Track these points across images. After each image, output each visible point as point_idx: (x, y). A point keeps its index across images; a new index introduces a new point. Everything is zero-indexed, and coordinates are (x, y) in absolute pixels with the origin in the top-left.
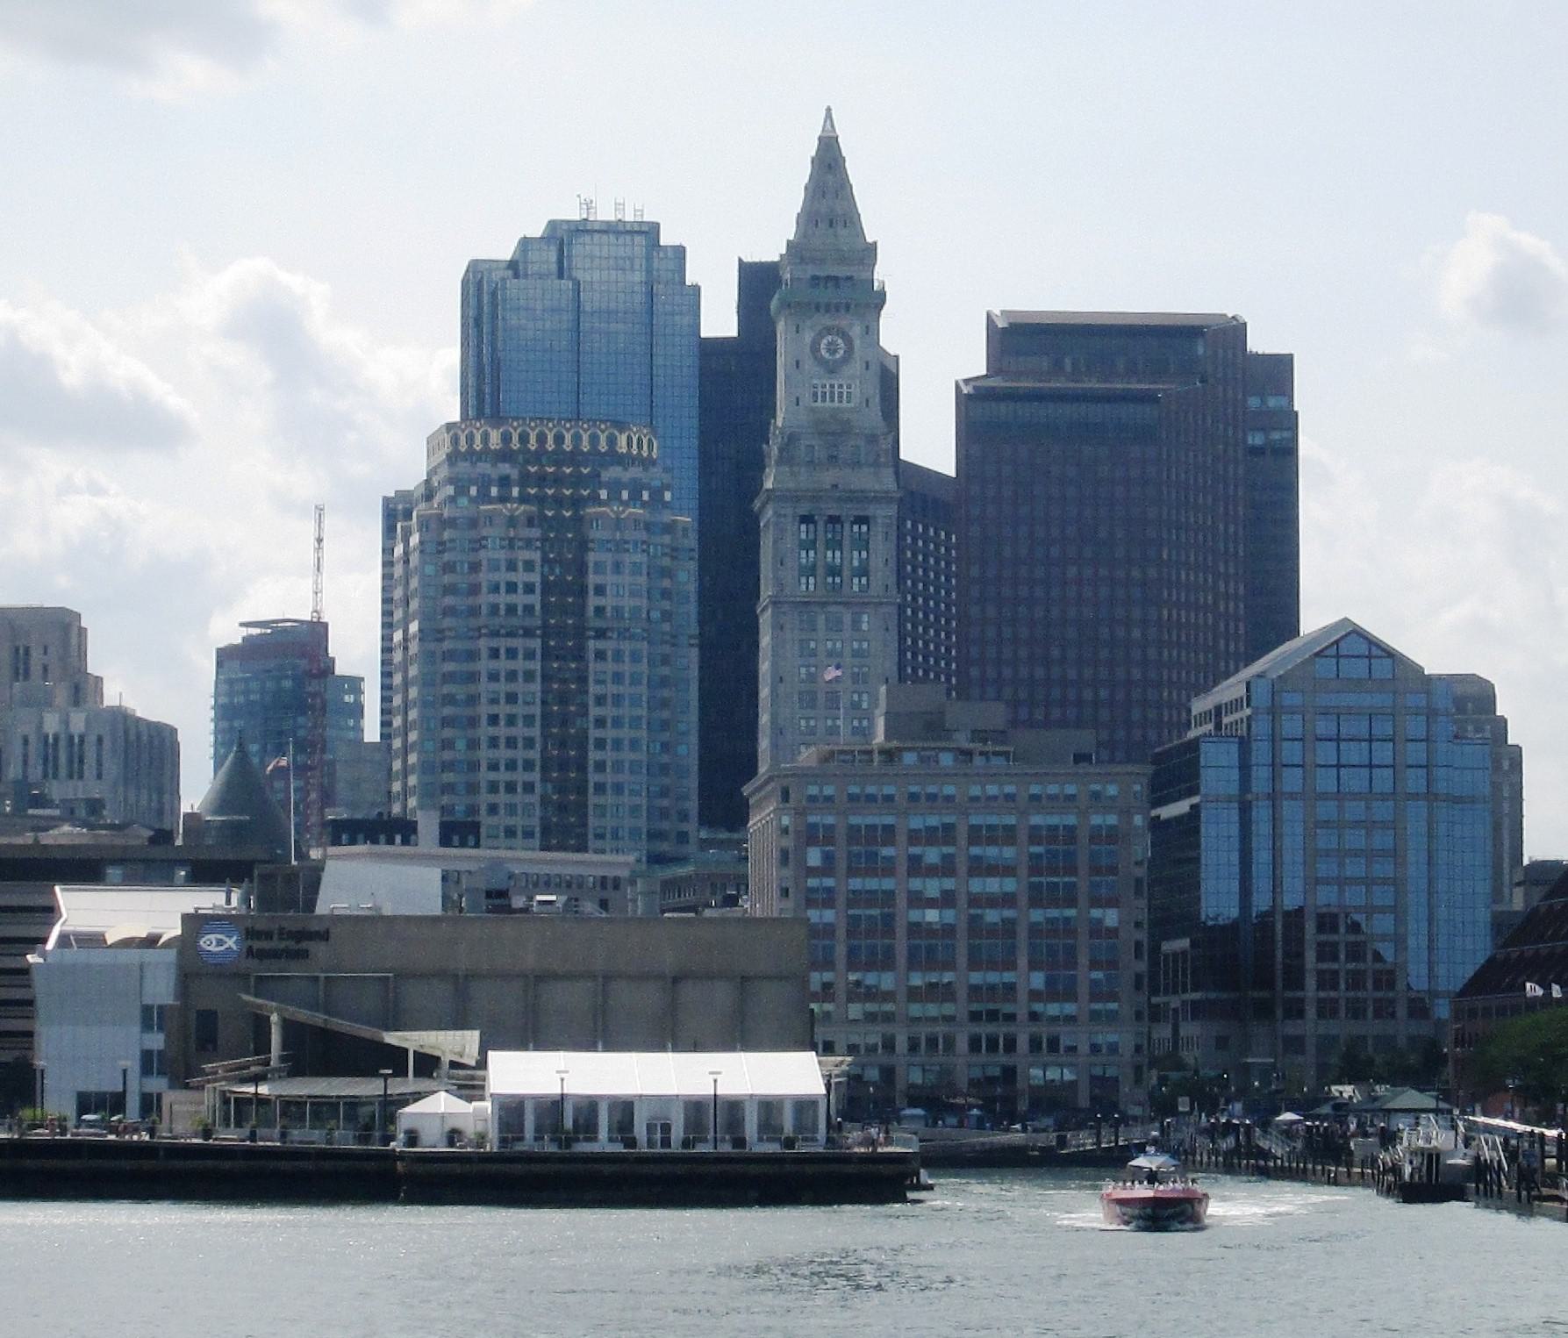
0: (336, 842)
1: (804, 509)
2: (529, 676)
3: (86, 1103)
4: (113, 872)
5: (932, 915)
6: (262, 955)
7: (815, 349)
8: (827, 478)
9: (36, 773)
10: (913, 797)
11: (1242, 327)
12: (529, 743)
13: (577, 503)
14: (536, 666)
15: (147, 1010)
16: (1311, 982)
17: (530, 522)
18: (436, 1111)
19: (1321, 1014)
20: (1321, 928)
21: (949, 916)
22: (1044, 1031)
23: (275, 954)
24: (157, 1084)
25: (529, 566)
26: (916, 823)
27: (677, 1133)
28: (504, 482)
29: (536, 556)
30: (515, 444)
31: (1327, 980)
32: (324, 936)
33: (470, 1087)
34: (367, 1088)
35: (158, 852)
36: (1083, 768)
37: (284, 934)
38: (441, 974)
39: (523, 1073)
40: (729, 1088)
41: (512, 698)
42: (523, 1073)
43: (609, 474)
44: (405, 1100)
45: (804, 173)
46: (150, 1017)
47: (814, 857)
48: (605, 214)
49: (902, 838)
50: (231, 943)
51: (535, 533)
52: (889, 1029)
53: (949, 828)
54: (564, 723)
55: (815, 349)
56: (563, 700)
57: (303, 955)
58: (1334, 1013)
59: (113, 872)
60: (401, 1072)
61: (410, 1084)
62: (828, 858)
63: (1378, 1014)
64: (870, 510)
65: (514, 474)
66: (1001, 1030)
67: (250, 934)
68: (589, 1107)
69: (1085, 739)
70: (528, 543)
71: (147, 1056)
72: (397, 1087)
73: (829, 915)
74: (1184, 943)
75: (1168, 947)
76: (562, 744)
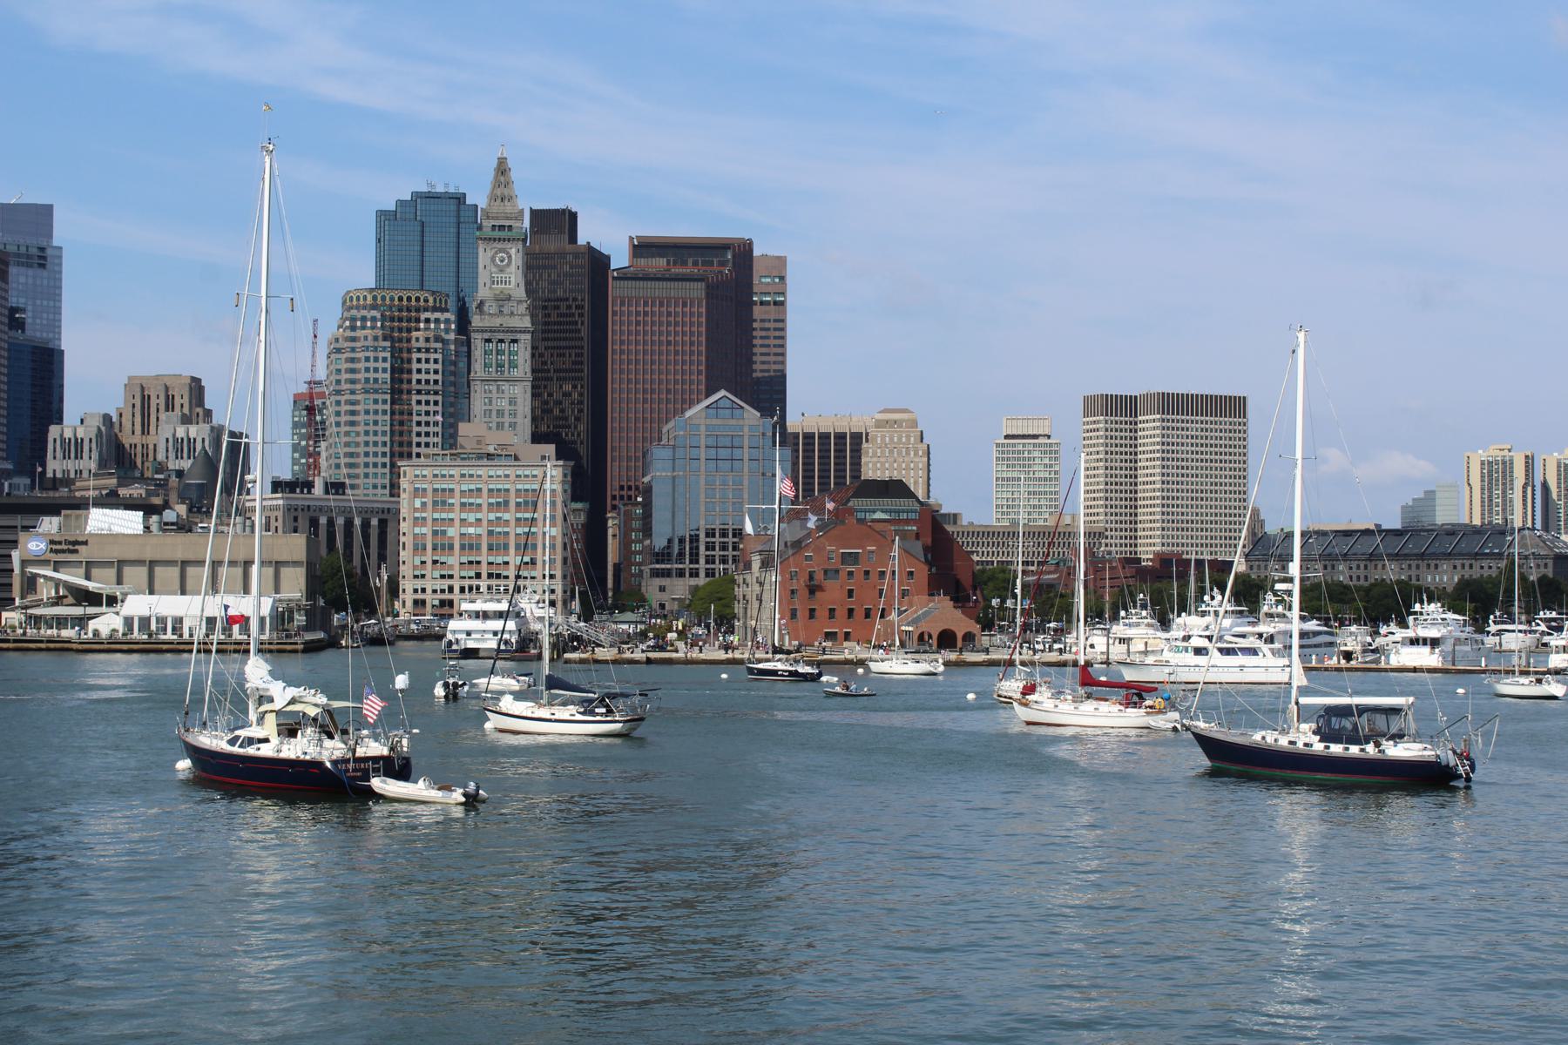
1: (486, 336)
2: (385, 412)
5: (471, 530)
6: (57, 551)
7: (493, 259)
8: (497, 322)
12: (385, 444)
13: (409, 330)
14: (388, 407)
16: (702, 561)
17: (385, 339)
18: (106, 623)
19: (707, 575)
20: (707, 535)
21: (479, 531)
23: (63, 551)
25: (385, 360)
26: (464, 488)
28: (374, 319)
29: (388, 355)
30: (379, 302)
32: (86, 543)
37: (67, 542)
38: (109, 564)
41: (376, 423)
42: (137, 605)
43: (423, 316)
45: (492, 174)
47: (418, 504)
48: (440, 189)
49: (457, 494)
50: (43, 546)
51: (388, 344)
52: (450, 582)
53: (479, 490)
54: (401, 434)
55: (493, 259)
56: (401, 423)
57: (76, 551)
58: (697, 575)
61: (104, 609)
62: (424, 504)
63: (691, 575)
64: (518, 336)
65: (378, 315)
66: (502, 582)
68: (162, 621)
70: (384, 349)
73: (424, 530)
76: (401, 444)
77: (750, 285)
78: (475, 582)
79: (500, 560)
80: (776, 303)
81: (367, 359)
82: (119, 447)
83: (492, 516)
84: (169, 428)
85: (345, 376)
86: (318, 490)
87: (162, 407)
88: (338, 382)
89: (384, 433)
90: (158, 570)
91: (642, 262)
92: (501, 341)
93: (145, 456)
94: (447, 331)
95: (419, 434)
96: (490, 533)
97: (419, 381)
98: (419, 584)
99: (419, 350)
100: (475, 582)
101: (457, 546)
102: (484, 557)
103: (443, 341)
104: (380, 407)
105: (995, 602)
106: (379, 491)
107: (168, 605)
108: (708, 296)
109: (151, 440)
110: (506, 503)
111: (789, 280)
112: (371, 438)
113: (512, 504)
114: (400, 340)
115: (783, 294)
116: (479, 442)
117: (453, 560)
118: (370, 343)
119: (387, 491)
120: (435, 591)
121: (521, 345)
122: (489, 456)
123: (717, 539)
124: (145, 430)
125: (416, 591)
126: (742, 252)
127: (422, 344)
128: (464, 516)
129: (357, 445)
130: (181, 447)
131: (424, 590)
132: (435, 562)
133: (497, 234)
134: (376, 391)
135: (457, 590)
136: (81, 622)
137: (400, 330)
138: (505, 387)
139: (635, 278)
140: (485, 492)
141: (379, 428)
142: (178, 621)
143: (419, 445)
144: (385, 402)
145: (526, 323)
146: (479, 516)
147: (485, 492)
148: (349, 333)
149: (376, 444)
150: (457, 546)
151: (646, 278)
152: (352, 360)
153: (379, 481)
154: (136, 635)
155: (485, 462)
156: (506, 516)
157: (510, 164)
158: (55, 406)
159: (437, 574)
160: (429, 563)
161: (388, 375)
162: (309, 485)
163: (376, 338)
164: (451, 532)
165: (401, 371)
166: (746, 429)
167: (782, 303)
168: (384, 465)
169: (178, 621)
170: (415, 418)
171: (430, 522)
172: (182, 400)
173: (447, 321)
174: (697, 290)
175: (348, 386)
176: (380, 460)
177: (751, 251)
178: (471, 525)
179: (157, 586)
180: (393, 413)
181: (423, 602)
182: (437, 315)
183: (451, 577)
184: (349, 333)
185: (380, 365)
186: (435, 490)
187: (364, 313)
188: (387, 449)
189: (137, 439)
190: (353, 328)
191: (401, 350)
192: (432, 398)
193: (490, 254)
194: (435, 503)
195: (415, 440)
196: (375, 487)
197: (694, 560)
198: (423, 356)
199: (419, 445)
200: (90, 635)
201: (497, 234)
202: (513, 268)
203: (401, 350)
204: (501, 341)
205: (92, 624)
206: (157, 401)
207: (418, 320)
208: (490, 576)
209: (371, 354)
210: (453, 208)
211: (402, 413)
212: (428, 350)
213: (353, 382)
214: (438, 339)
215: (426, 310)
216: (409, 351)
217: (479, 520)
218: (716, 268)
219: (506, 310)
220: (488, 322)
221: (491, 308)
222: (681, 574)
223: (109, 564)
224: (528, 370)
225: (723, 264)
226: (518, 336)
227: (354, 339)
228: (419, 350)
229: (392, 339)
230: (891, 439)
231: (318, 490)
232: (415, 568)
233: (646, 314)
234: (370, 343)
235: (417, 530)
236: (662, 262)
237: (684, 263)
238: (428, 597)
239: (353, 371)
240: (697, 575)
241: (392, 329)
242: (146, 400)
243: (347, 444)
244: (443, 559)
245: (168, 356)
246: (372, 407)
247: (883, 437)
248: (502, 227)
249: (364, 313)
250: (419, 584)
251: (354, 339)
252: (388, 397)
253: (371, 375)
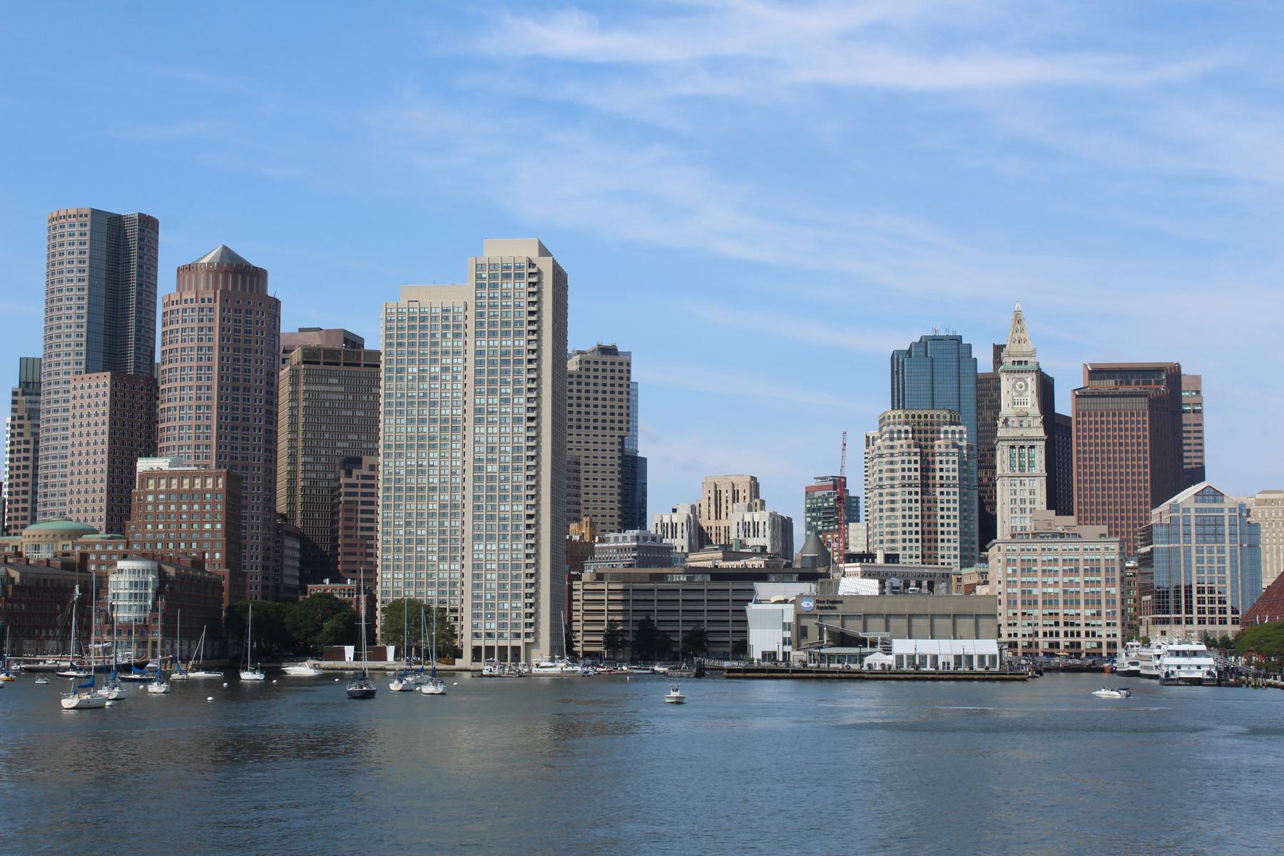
0: (848, 562)
1: (1011, 443)
2: (916, 501)
3: (764, 654)
4: (773, 578)
5: (1050, 590)
6: (821, 608)
8: (1018, 433)
9: (742, 537)
10: (1043, 549)
11: (1179, 367)
12: (917, 525)
13: (932, 440)
14: (919, 497)
15: (784, 624)
16: (1195, 611)
18: (877, 659)
19: (1199, 623)
21: (1057, 590)
22: (1090, 629)
23: (826, 608)
24: (788, 648)
25: (916, 462)
26: (1045, 558)
27: (952, 665)
28: (907, 432)
29: (918, 458)
31: (1201, 611)
32: (841, 602)
33: (888, 651)
34: (855, 650)
35: (788, 570)
36: (1103, 539)
37: (829, 602)
38: (879, 615)
39: (903, 646)
40: (969, 651)
41: (910, 509)
42: (903, 646)
43: (943, 429)
44: (866, 655)
46: (786, 626)
47: (1010, 570)
48: (942, 333)
49: (1039, 563)
50: (811, 604)
53: (1056, 560)
54: (929, 517)
55: (1014, 386)
58: (1225, 623)
59: (773, 578)
60: (865, 646)
61: (868, 649)
62: (1014, 571)
63: (1199, 623)
64: (1034, 443)
66: (1075, 629)
67: (818, 601)
68: (923, 657)
69: (1104, 529)
71: (784, 639)
72: (864, 650)
73: (1015, 590)
74: (1149, 597)
75: (1144, 598)
76: (929, 525)
77: (1180, 398)
78: (1054, 629)
79: (1072, 612)
80: (1194, 411)
81: (903, 462)
82: (701, 528)
83: (1066, 579)
84: (737, 516)
85: (885, 475)
86: (880, 560)
87: (730, 500)
88: (881, 479)
89: (917, 517)
90: (959, 621)
91: (1096, 383)
92: (1022, 447)
93: (718, 535)
94: (961, 440)
95: (942, 517)
96: (1065, 592)
97: (941, 478)
98: (1012, 630)
99: (941, 454)
100: (1054, 629)
101: (1040, 603)
102: (1061, 611)
103: (960, 448)
104: (913, 497)
105: (196, 507)
106: (914, 560)
107: (926, 647)
108: (1150, 408)
109: (723, 523)
110: (1077, 570)
111: (1203, 393)
112: (907, 521)
113: (1081, 571)
114: (926, 447)
115: (1200, 404)
116: (1049, 524)
117: (1038, 612)
118: (905, 449)
119: (920, 560)
120: (1024, 636)
121: (1037, 449)
122: (1062, 535)
123: (1206, 595)
124: (718, 517)
125: (1010, 635)
126: (1173, 375)
127: (943, 450)
128: (1045, 579)
129: (896, 525)
130: (751, 529)
131: (1016, 635)
132: (1024, 614)
133: (1017, 367)
134: (910, 485)
135: (1083, 634)
136: (862, 657)
137: (926, 440)
138: (1027, 481)
139: (1092, 396)
140: (1060, 562)
141: (913, 513)
142: (935, 658)
143: (942, 525)
144: (916, 493)
145: (1041, 433)
146: (1056, 579)
147: (1060, 562)
148: (888, 443)
149: (910, 525)
150: (1040, 603)
151: (1101, 395)
152: (892, 463)
153: (914, 553)
154: (905, 668)
155: (1058, 539)
156: (1077, 579)
157: (1024, 315)
158: (638, 499)
159: (1025, 623)
160: (1019, 615)
161: (918, 474)
162: (873, 557)
163: (909, 446)
164: (1035, 591)
165: (928, 470)
166: (1226, 511)
167: (1200, 411)
168: (917, 541)
169: (935, 658)
170: (939, 505)
171: (1019, 584)
172: (744, 492)
173: (961, 432)
174: (1142, 404)
175: (890, 482)
176: (914, 537)
177: (1180, 371)
178: (1050, 586)
179: (936, 634)
180: (923, 502)
181: (1057, 645)
182: (953, 428)
183: (1036, 625)
184: (888, 443)
185: (913, 466)
186: (1023, 561)
187: (900, 427)
188: (919, 529)
189: (712, 523)
190: (892, 439)
191: (927, 455)
192: (951, 490)
193: (1011, 382)
194: (1023, 570)
195: (940, 521)
196: (911, 557)
197: (1189, 610)
198: (944, 458)
199: (942, 525)
200: (865, 668)
201: (1017, 367)
202: (1029, 392)
203: (927, 455)
204: (1022, 447)
205: (867, 660)
206: (726, 495)
207: (939, 432)
208: (1066, 624)
209: (906, 458)
210: (955, 347)
211: (929, 501)
212: (947, 454)
213: (892, 479)
214: (954, 446)
215: (945, 424)
216: (933, 455)
217: (1056, 583)
218: (1153, 386)
219: (1024, 424)
220: (1011, 433)
221: (1014, 422)
222: (1178, 621)
223: (879, 615)
224: (1043, 467)
225: (1158, 383)
226: (1034, 443)
227: (892, 447)
228: (941, 454)
229: (920, 447)
230: (1270, 514)
231: (880, 560)
232: (1009, 618)
233: (1102, 422)
234: (905, 449)
235: (1010, 590)
236: (1111, 383)
237: (1129, 383)
238: (1019, 640)
239: (892, 471)
240: (1225, 623)
241: (920, 439)
242: (718, 494)
243: (889, 525)
244: (1030, 612)
245: (736, 466)
246: (907, 497)
247: (1263, 513)
248: (1020, 363)
249: (900, 427)
250: (1012, 630)
251: (892, 447)
252: (919, 490)
253: (906, 474)
